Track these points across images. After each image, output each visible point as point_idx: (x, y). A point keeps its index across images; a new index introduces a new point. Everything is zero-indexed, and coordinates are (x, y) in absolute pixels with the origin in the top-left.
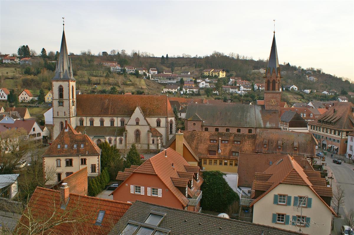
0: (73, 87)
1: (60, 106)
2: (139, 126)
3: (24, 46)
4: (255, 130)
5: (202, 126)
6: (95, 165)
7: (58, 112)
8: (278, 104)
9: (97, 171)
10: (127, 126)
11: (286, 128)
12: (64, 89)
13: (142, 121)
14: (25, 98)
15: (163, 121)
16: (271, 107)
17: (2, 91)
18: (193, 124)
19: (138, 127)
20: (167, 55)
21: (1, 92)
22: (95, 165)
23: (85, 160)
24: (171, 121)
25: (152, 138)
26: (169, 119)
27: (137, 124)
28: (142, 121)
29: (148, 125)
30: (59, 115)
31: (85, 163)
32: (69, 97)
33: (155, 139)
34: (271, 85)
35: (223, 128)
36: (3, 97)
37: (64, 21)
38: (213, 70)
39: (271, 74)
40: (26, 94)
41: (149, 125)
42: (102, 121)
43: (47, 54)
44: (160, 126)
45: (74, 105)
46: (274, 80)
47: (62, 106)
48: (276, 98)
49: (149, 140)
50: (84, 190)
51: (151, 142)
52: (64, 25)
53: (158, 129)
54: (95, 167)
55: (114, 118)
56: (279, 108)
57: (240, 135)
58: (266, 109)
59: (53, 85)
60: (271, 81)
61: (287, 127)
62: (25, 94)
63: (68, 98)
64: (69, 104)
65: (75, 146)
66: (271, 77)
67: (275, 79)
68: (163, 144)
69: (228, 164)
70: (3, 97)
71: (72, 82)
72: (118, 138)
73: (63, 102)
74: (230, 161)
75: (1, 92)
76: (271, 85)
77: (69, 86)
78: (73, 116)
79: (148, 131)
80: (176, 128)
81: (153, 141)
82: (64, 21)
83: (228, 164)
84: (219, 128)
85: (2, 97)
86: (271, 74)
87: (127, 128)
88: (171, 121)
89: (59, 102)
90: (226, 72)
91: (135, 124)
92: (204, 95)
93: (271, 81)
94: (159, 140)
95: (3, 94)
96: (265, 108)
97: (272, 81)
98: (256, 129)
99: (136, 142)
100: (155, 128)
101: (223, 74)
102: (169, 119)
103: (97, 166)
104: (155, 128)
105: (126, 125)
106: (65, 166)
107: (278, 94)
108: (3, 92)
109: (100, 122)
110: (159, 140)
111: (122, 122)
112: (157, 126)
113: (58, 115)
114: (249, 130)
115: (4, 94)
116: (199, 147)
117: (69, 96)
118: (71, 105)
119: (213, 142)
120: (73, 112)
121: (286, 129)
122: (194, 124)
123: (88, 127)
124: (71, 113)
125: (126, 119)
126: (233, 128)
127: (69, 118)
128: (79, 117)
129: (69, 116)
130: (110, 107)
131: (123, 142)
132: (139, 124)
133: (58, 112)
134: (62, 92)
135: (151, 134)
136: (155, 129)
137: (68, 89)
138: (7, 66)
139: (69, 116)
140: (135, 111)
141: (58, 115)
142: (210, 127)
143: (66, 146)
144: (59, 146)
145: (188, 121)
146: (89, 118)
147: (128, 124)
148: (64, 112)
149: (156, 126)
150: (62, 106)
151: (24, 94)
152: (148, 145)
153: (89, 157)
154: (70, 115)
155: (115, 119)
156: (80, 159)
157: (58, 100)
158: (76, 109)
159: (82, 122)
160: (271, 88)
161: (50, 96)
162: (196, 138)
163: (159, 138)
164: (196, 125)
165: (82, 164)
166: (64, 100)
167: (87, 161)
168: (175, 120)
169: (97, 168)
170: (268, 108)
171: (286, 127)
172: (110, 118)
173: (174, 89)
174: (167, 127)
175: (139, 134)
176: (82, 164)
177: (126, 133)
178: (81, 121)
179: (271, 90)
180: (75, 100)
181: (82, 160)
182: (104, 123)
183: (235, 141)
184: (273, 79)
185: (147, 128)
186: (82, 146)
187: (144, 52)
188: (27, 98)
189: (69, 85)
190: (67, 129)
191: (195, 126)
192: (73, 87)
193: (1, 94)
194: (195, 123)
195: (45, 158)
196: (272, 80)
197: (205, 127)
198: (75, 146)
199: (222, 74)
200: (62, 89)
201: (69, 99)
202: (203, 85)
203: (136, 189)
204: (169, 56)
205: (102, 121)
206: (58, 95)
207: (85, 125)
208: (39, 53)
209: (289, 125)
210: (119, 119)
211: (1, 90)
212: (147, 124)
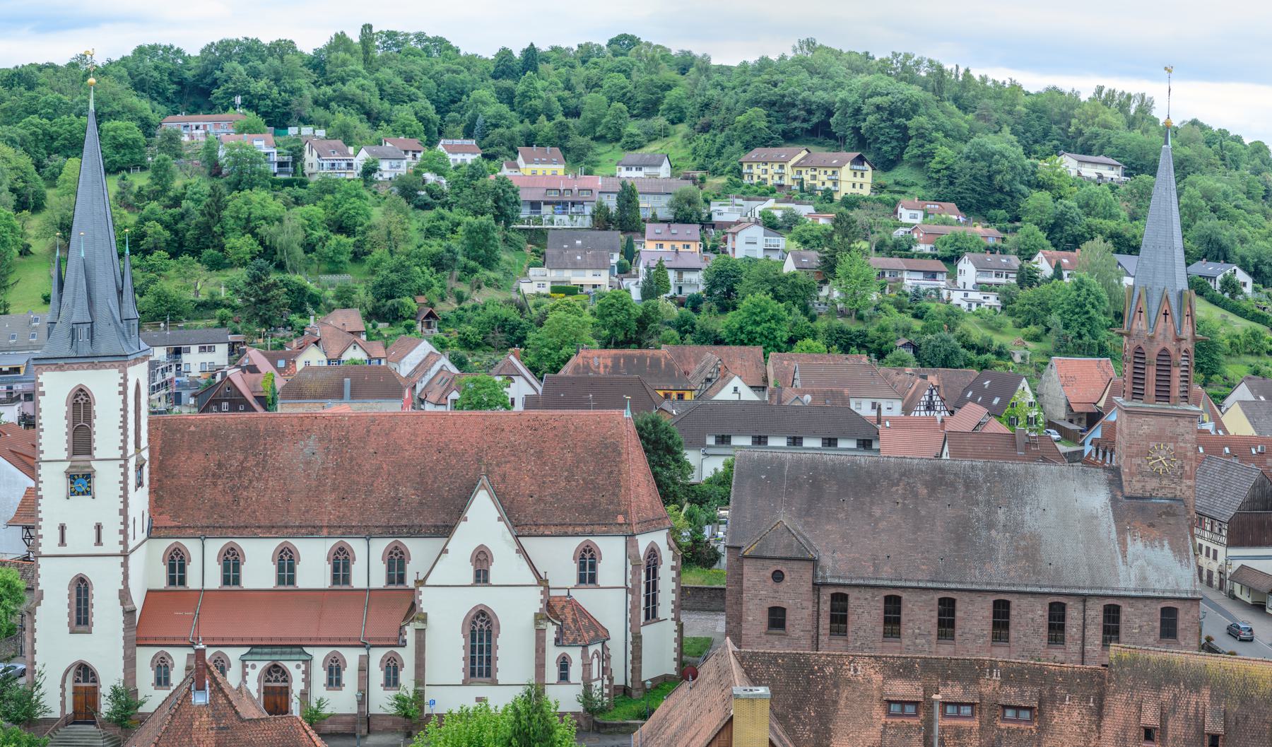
0: (138, 386)
4: (1081, 607)
5: (817, 587)
7: (62, 528)
8: (1187, 468)
11: (1213, 546)
13: (506, 565)
15: (611, 550)
16: (1152, 484)
18: (769, 574)
19: (482, 596)
24: (653, 553)
26: (643, 542)
27: (481, 577)
28: (506, 565)
29: (536, 582)
32: (124, 448)
33: (575, 654)
34: (1151, 373)
35: (925, 597)
38: (804, 153)
39: (1153, 322)
41: (539, 584)
44: (593, 579)
46: (1165, 350)
48: (1174, 439)
51: (552, 672)
53: (585, 597)
55: (351, 542)
56: (1189, 487)
58: (1127, 490)
59: (41, 389)
60: (1152, 353)
61: (1221, 544)
64: (125, 475)
66: (1151, 339)
67: (1172, 347)
72: (377, 655)
73: (88, 477)
76: (1151, 373)
77: (124, 393)
80: (678, 585)
81: (564, 665)
84: (904, 596)
86: (1153, 322)
87: (428, 600)
89: (72, 478)
90: (874, 169)
91: (471, 580)
93: (1152, 353)
94: (595, 661)
96: (1125, 484)
97: (1155, 357)
98: (1084, 601)
99: (473, 674)
101: (858, 179)
102: (643, 542)
107: (1182, 422)
110: (595, 661)
111: (396, 563)
112: (582, 579)
114: (1051, 605)
117: (125, 441)
121: (1215, 552)
122: (778, 576)
124: (130, 522)
125: (419, 550)
126: (973, 595)
128: (167, 543)
129: (121, 547)
132: (492, 580)
133: (62, 528)
135: (551, 631)
137: (121, 406)
139: (121, 547)
142: (857, 590)
145: (746, 562)
146: (215, 547)
149: (573, 579)
150: (88, 492)
154: (124, 543)
159: (177, 565)
160: (1151, 389)
163: (596, 652)
164: (783, 584)
166: (94, 464)
168: (671, 548)
170: (1138, 486)
171: (1211, 540)
173: (589, 273)
175: (489, 632)
177: (420, 633)
179: (1153, 397)
180: (145, 455)
183: (1005, 707)
184: (1161, 347)
185: (533, 601)
189: (125, 378)
190: (204, 689)
191: (782, 586)
192: (138, 386)
194: (784, 570)
196: (1157, 351)
197: (833, 590)
199: (855, 180)
201: (125, 458)
207: (193, 582)
209: (1229, 536)
212: (532, 579)
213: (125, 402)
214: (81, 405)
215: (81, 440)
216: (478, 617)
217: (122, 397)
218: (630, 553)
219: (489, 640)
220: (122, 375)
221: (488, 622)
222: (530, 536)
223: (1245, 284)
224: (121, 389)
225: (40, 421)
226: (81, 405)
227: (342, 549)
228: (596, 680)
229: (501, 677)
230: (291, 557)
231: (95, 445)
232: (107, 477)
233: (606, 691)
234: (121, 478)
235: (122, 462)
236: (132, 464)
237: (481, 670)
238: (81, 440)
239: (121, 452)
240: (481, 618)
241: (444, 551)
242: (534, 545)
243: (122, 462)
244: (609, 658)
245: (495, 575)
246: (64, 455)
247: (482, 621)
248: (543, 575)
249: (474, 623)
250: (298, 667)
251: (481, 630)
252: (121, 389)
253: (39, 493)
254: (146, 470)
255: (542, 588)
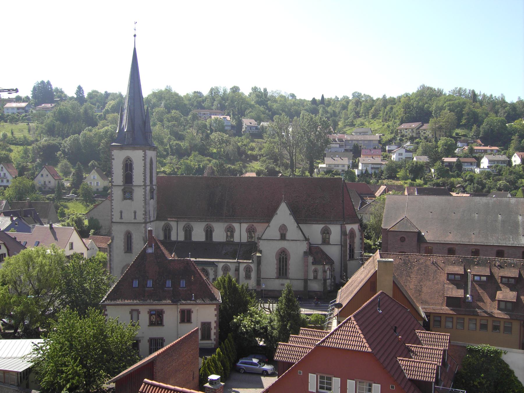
1: (125, 198)
2: (286, 242)
3: (43, 82)
6: (209, 324)
7: (121, 212)
9: (213, 337)
10: (261, 242)
12: (135, 166)
14: (47, 183)
15: (335, 230)
17: (4, 168)
19: (284, 244)
20: (323, 95)
21: (2, 170)
22: (209, 324)
23: (189, 312)
24: (352, 232)
25: (313, 267)
27: (283, 237)
29: (305, 239)
30: (123, 217)
31: (189, 321)
33: (320, 268)
36: (5, 181)
37: (135, 30)
40: (49, 175)
42: (209, 230)
43: (86, 95)
45: (152, 198)
47: (131, 199)
49: (306, 272)
50: (191, 378)
52: (135, 36)
53: (326, 249)
54: (209, 329)
57: (514, 264)
62: (47, 175)
63: (142, 184)
65: (169, 283)
68: (335, 279)
69: (490, 327)
70: (5, 181)
71: (150, 150)
74: (493, 321)
75: (2, 170)
78: (152, 219)
79: (305, 253)
82: (135, 30)
83: (490, 327)
85: (2, 181)
88: (352, 232)
89: (124, 192)
91: (279, 238)
92: (405, 178)
94: (328, 272)
95: (5, 174)
100: (320, 246)
102: (349, 227)
103: (213, 325)
104: (319, 246)
105: (259, 239)
106: (148, 325)
108: (5, 171)
109: (204, 234)
110: (328, 272)
111: (251, 231)
113: (121, 218)
115: (7, 174)
116: (425, 289)
118: (147, 198)
119: (480, 278)
120: (152, 213)
123: (181, 242)
125: (259, 227)
127: (144, 225)
130: (226, 201)
131: (253, 275)
132: (287, 238)
133: (121, 212)
134: (132, 171)
135: (310, 259)
136: (319, 248)
138: (14, 120)
139: (144, 220)
140: (278, 212)
141: (121, 218)
143: (150, 283)
144: (136, 284)
147: (263, 238)
148: (133, 211)
149: (320, 241)
150: (131, 199)
151: (44, 175)
152: (306, 281)
153: (197, 307)
155: (236, 226)
156: (179, 310)
157: (123, 187)
158: (156, 206)
161: (94, 179)
162: (416, 268)
164: (407, 240)
165: (183, 321)
167: (194, 316)
169: (213, 331)
172: (226, 225)
174: (343, 245)
175: (286, 258)
176: (183, 321)
178: (166, 229)
181: (183, 312)
182: (214, 234)
185: (304, 247)
186: (183, 283)
187: (274, 90)
188: (50, 182)
193: (2, 175)
194: (405, 237)
195: (107, 307)
198: (169, 283)
200: (131, 165)
202: (401, 157)
203: (321, 382)
204: (326, 97)
205: (209, 230)
206: (122, 177)
208: (71, 92)
210: (245, 226)
211: (2, 168)
212: (301, 237)
213: (145, 164)
214: (128, 166)
215: (128, 178)
216: (282, 253)
217: (144, 161)
218: (343, 233)
219: (286, 262)
220: (144, 153)
221: (286, 255)
222: (301, 224)
223: (90, 131)
224: (143, 158)
225: (113, 170)
226: (128, 166)
227: (230, 227)
228: (328, 279)
229: (290, 276)
230: (211, 229)
231: (134, 180)
232: (139, 194)
233: (332, 284)
234: (144, 194)
235: (144, 187)
236: (148, 188)
237: (283, 273)
238: (128, 178)
239: (143, 183)
240: (283, 253)
241: (268, 226)
242: (303, 226)
243: (144, 187)
244: (334, 270)
245: (288, 236)
246: (122, 184)
247: (283, 254)
248: (307, 238)
249: (280, 255)
250: (212, 269)
251: (283, 258)
252: (143, 158)
253: (112, 198)
254: (155, 192)
255: (307, 242)
